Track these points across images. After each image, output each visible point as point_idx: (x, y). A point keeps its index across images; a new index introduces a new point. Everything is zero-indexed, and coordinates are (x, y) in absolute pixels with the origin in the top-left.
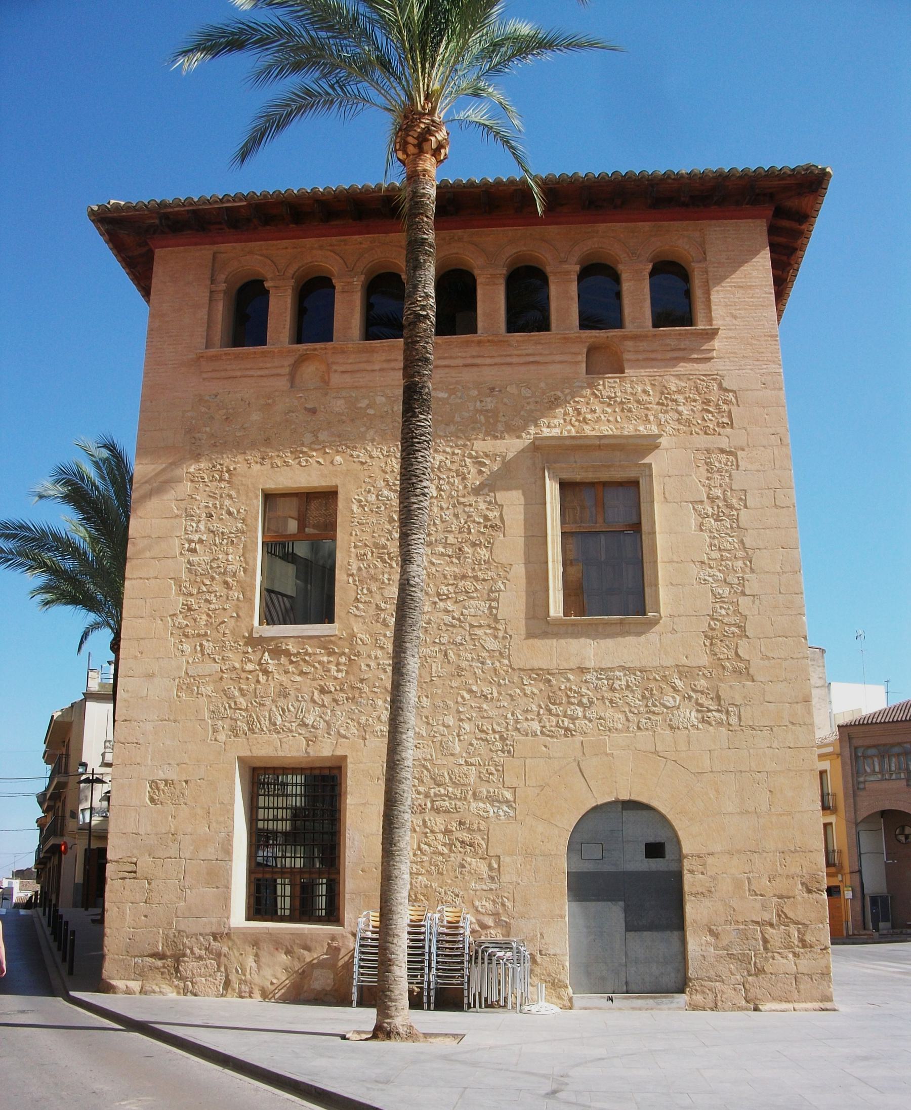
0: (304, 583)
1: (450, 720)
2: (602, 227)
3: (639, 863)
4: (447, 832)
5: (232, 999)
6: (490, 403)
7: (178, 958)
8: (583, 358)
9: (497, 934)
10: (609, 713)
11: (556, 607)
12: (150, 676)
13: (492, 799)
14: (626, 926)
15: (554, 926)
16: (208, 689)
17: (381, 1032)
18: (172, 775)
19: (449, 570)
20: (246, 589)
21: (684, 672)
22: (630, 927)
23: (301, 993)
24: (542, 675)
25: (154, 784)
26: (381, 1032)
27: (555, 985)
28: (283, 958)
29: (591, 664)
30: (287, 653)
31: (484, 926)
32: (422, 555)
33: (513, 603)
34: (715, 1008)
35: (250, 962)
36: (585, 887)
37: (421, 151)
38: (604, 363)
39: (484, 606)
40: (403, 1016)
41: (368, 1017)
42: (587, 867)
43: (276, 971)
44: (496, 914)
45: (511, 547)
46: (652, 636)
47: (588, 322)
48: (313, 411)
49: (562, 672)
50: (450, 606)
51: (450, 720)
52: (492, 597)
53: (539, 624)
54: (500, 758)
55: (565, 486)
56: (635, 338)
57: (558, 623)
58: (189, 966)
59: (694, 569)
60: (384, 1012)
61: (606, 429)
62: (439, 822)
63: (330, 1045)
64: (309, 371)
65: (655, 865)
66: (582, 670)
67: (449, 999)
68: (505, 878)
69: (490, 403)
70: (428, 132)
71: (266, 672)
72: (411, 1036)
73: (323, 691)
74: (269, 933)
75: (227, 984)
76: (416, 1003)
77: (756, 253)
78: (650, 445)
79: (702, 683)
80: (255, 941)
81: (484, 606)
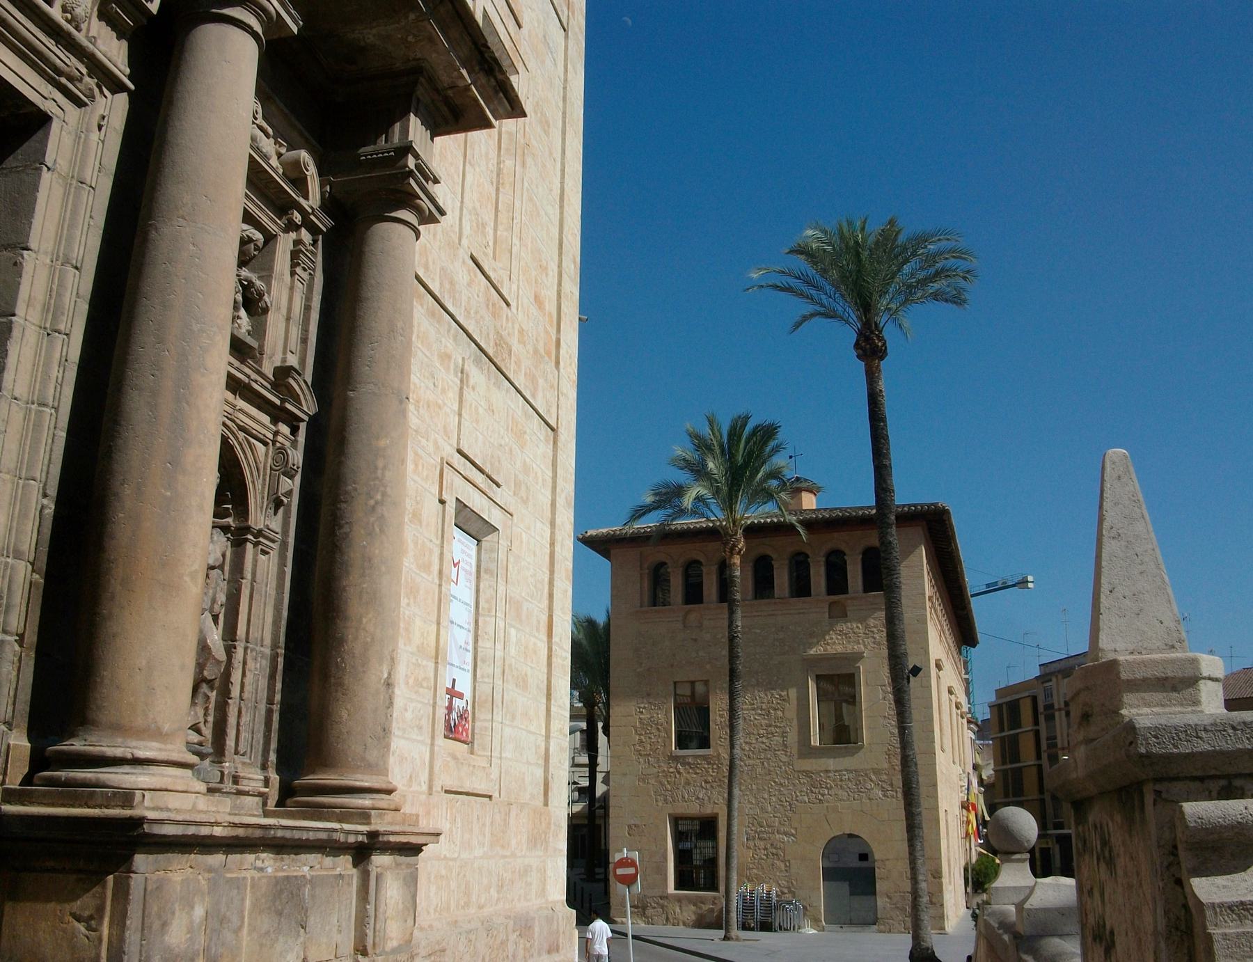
0: (694, 732)
1: (766, 796)
2: (836, 535)
3: (856, 863)
4: (766, 849)
5: (669, 927)
6: (781, 635)
7: (644, 908)
8: (827, 610)
9: (788, 897)
10: (840, 792)
11: (815, 741)
12: (625, 775)
13: (785, 834)
14: (866, 894)
15: (819, 893)
16: (652, 781)
17: (726, 938)
18: (637, 822)
19: (764, 722)
20: (668, 732)
21: (877, 772)
22: (852, 894)
23: (702, 923)
24: (807, 774)
25: (630, 827)
26: (726, 938)
27: (816, 921)
28: (693, 908)
29: (831, 768)
30: (689, 764)
31: (783, 893)
32: (740, 739)
33: (793, 737)
34: (890, 932)
35: (678, 910)
36: (830, 874)
37: (732, 554)
38: (838, 614)
39: (780, 740)
40: (735, 932)
41: (722, 933)
42: (831, 865)
43: (689, 913)
44: (789, 888)
45: (791, 711)
46: (861, 754)
47: (830, 591)
48: (695, 640)
49: (818, 773)
50: (764, 740)
51: (766, 796)
52: (784, 735)
53: (806, 751)
54: (790, 814)
55: (819, 678)
56: (852, 598)
57: (815, 748)
58: (649, 911)
59: (881, 720)
60: (727, 931)
61: (839, 649)
62: (762, 844)
63: (710, 940)
64: (693, 617)
65: (864, 864)
66: (827, 771)
67: (766, 927)
68: (793, 871)
69: (781, 635)
70: (734, 546)
71: (679, 773)
72: (738, 939)
73: (706, 782)
74: (686, 897)
75: (667, 919)
76: (745, 927)
77: (916, 546)
78: (859, 657)
79: (885, 777)
80: (679, 900)
81: (780, 740)
